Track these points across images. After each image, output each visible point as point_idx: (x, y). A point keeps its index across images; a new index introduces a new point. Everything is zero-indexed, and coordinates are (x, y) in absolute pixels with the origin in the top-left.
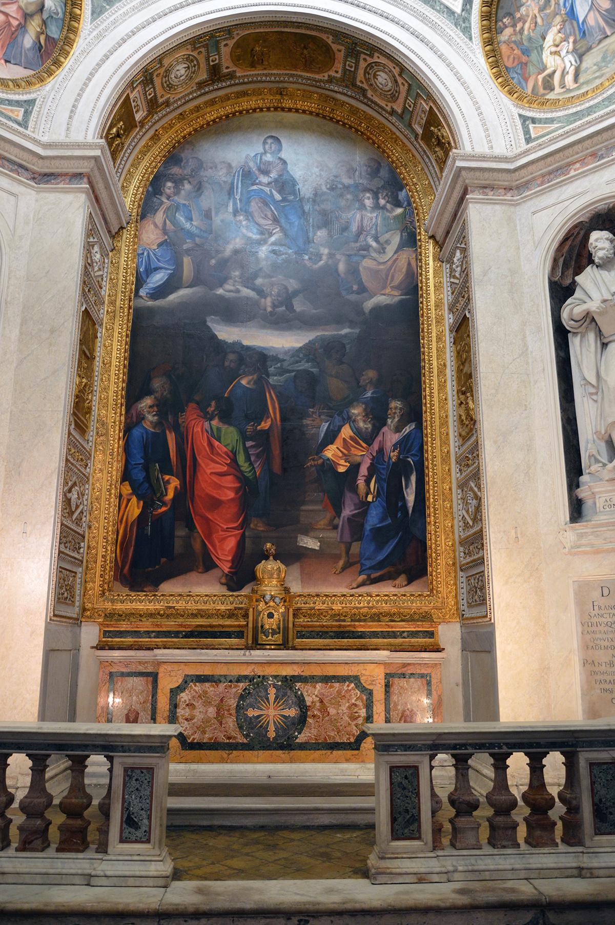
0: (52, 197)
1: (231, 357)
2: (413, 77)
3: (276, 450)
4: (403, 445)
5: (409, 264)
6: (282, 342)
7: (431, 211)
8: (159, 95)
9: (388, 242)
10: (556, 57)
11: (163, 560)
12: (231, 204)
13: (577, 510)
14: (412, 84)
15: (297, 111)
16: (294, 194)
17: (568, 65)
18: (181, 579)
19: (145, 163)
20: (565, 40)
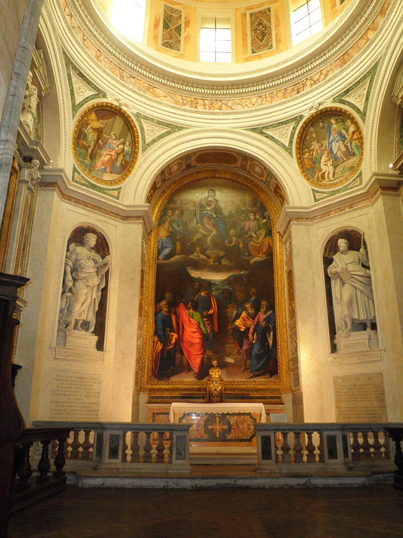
0: (129, 225)
1: (197, 284)
2: (269, 171)
3: (216, 322)
4: (268, 319)
5: (269, 243)
6: (217, 277)
7: (278, 227)
8: (166, 177)
9: (260, 234)
10: (326, 166)
11: (171, 367)
12: (195, 220)
13: (334, 348)
14: (268, 174)
15: (222, 178)
16: (221, 215)
17: (330, 170)
18: (176, 376)
19: (160, 203)
20: (329, 160)
